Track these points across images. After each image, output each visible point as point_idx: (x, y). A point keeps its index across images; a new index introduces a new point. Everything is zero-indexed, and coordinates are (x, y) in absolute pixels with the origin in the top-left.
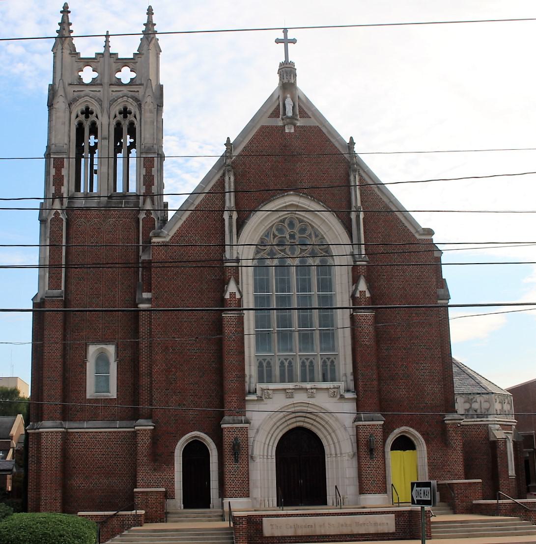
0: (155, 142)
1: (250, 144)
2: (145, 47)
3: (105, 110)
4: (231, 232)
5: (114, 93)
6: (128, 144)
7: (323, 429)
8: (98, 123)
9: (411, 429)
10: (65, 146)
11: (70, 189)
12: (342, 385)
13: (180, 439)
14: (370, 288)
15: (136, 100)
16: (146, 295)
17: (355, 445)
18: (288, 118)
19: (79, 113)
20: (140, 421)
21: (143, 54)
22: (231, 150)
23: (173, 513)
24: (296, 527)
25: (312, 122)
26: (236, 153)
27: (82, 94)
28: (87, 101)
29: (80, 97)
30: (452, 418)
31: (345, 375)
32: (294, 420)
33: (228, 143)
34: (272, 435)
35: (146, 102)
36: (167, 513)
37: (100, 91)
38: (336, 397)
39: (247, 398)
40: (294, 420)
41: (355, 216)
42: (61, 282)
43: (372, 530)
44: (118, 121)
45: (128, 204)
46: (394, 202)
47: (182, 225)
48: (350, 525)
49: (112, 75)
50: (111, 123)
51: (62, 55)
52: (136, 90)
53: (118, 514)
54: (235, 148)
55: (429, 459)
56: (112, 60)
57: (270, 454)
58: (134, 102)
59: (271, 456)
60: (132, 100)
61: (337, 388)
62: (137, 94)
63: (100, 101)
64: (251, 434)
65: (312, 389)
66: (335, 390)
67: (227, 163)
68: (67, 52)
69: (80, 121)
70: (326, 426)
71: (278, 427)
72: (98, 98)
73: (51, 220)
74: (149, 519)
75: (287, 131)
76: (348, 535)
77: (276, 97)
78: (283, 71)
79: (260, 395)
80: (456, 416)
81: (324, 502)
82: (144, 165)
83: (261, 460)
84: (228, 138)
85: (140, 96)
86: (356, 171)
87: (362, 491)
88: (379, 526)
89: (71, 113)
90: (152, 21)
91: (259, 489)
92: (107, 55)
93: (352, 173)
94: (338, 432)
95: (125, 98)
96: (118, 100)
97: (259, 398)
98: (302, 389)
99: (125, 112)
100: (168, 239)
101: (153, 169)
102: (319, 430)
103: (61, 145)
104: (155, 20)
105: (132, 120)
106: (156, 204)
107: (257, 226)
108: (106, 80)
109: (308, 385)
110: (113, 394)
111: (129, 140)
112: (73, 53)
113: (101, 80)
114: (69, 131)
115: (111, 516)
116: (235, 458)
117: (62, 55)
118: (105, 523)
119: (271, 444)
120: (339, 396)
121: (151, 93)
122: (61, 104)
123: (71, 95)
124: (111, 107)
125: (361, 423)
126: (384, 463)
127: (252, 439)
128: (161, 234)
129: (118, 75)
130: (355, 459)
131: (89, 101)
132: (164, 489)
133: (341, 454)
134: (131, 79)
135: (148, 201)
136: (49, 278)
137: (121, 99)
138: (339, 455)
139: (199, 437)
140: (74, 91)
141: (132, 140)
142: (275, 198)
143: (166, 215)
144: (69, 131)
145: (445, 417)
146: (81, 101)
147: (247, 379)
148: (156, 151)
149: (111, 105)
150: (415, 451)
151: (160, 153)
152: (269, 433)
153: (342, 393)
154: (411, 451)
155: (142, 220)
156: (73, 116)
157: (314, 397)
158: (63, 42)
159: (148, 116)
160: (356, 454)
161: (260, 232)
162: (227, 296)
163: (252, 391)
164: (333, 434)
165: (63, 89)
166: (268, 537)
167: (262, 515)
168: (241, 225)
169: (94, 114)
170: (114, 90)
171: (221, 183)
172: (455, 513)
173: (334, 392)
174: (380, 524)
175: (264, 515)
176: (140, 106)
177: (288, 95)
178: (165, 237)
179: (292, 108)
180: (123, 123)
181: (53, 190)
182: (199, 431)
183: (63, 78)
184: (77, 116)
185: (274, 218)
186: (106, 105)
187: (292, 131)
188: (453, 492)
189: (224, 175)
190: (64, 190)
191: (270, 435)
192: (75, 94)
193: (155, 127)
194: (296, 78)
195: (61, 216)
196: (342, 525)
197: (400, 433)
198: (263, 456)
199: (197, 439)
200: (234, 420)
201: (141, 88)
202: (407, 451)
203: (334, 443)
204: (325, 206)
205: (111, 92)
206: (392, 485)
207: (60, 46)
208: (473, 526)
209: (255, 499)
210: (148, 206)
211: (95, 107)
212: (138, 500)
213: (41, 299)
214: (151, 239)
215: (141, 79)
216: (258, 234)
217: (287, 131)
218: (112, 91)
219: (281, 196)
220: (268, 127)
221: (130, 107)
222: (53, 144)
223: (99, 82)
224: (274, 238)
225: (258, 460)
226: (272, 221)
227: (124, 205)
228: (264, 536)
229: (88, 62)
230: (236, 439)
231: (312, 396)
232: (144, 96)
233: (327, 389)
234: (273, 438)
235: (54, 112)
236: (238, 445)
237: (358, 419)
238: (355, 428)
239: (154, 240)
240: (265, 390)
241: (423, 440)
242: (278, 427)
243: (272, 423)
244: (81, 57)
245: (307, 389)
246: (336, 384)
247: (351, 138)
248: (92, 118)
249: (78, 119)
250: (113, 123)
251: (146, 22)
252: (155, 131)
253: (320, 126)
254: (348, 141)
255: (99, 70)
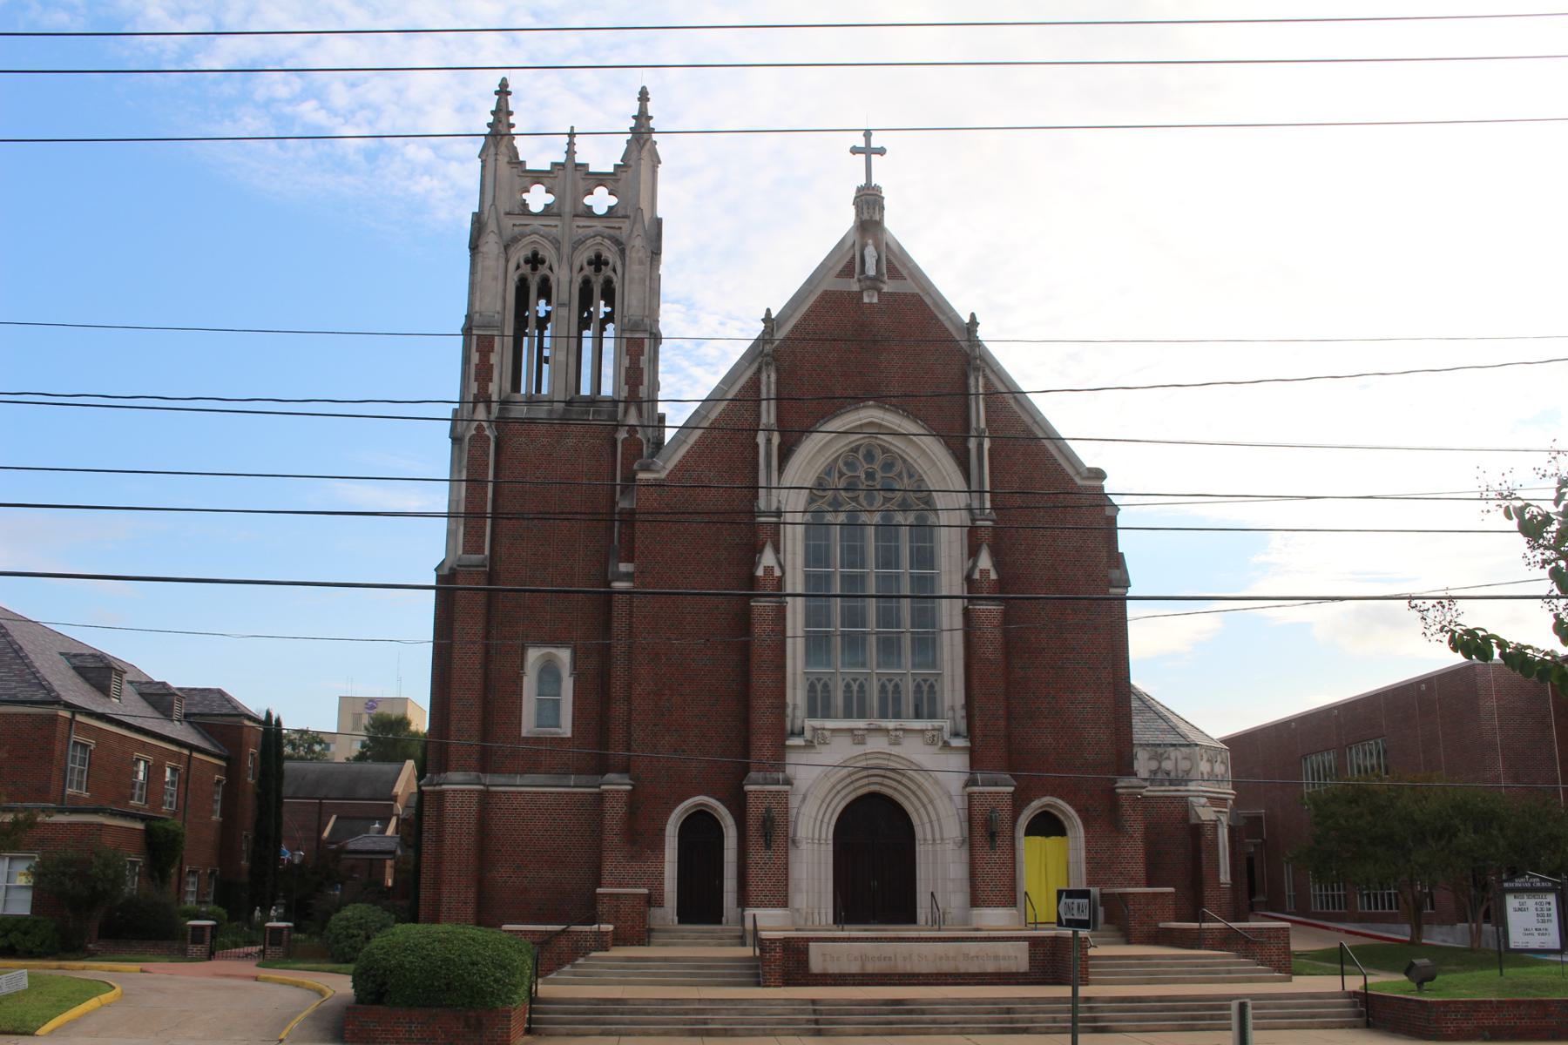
0: (647, 313)
1: (805, 320)
2: (634, 155)
3: (565, 258)
4: (768, 465)
5: (580, 231)
6: (602, 316)
7: (913, 798)
8: (553, 279)
9: (1060, 802)
10: (496, 316)
11: (503, 388)
12: (947, 725)
13: (676, 806)
14: (997, 565)
15: (617, 242)
16: (624, 567)
17: (966, 825)
18: (868, 278)
19: (522, 262)
20: (610, 776)
21: (630, 166)
22: (773, 330)
23: (660, 931)
24: (864, 958)
25: (908, 287)
26: (781, 334)
27: (527, 230)
28: (535, 241)
29: (523, 235)
30: (1129, 785)
31: (953, 708)
32: (866, 781)
33: (767, 319)
34: (828, 806)
35: (634, 246)
36: (651, 930)
37: (556, 226)
38: (935, 745)
39: (789, 743)
40: (866, 781)
41: (976, 445)
42: (484, 542)
43: (990, 967)
44: (586, 276)
45: (599, 415)
46: (1041, 423)
47: (688, 452)
48: (955, 958)
49: (577, 200)
50: (574, 280)
51: (496, 165)
52: (617, 225)
53: (568, 929)
54: (779, 327)
55: (1088, 852)
56: (579, 175)
57: (824, 836)
58: (613, 245)
59: (826, 840)
60: (609, 242)
61: (939, 730)
62: (618, 232)
63: (556, 243)
64: (794, 802)
65: (896, 730)
66: (936, 733)
67: (765, 352)
68: (503, 160)
69: (522, 274)
70: (920, 793)
71: (838, 792)
72: (554, 238)
73: (470, 439)
74: (620, 939)
75: (866, 300)
76: (951, 974)
77: (849, 243)
78: (861, 200)
79: (809, 738)
80: (1134, 781)
81: (911, 918)
82: (628, 350)
83: (809, 845)
84: (768, 310)
85: (623, 235)
86: (979, 371)
87: (975, 902)
88: (1002, 962)
89: (507, 261)
90: (646, 112)
91: (805, 894)
92: (570, 167)
93: (972, 372)
94: (938, 802)
95: (599, 239)
96: (588, 241)
97: (809, 744)
98: (879, 730)
99: (598, 262)
100: (663, 475)
101: (642, 358)
102: (907, 798)
103: (491, 314)
104: (652, 109)
105: (609, 277)
106: (646, 417)
107: (813, 457)
108: (568, 208)
109: (891, 724)
110: (566, 729)
111: (603, 309)
112: (514, 161)
113: (559, 208)
114: (505, 290)
115: (557, 933)
116: (766, 841)
117: (496, 165)
118: (546, 944)
119: (826, 820)
120: (940, 744)
121: (641, 232)
122: (491, 245)
123: (509, 232)
124: (575, 254)
125: (975, 789)
126: (1014, 858)
127: (796, 810)
128: (653, 467)
129: (588, 200)
130: (966, 846)
131: (539, 243)
132: (646, 891)
133: (942, 839)
134: (546, 205)
135: (633, 411)
136: (464, 534)
137: (592, 240)
138: (939, 842)
139: (712, 808)
140: (514, 225)
141: (608, 309)
142: (842, 411)
143: (661, 435)
144: (505, 290)
145: (1116, 783)
146: (525, 241)
147: (789, 711)
148: (648, 328)
149: (574, 249)
150: (1065, 837)
151: (654, 331)
152: (823, 802)
153: (946, 738)
154: (1059, 837)
155: (622, 442)
156: (512, 266)
157: (899, 744)
158: (498, 143)
159: (635, 270)
160: (967, 839)
161: (817, 466)
162: (760, 572)
163: (796, 730)
164: (930, 807)
165: (495, 221)
166: (816, 975)
167: (807, 938)
168: (785, 454)
169: (547, 264)
170: (581, 224)
171: (755, 383)
172: (1129, 942)
173: (934, 736)
174: (1004, 958)
175: (812, 938)
176: (622, 252)
177: (870, 241)
178: (658, 472)
179: (875, 262)
180: (593, 279)
181: (474, 388)
182: (707, 795)
183: (497, 203)
184: (518, 267)
185: (842, 444)
186: (566, 249)
187: (875, 300)
188: (1126, 906)
189: (759, 370)
190: (493, 388)
191: (825, 805)
192: (516, 229)
193: (648, 289)
194: (883, 212)
195: (487, 432)
196: (941, 958)
197: (1041, 807)
198: (813, 839)
199: (703, 808)
200: (766, 779)
201: (624, 222)
202: (1053, 838)
203: (931, 822)
204: (925, 426)
205: (575, 229)
206: (1026, 893)
207: (492, 150)
208: (1158, 965)
209: (798, 910)
210: (632, 420)
211: (548, 252)
212: (602, 908)
213: (451, 569)
214: (635, 473)
215: (626, 209)
216: (814, 470)
217: (866, 300)
218: (578, 227)
219: (853, 407)
220: (834, 293)
221: (606, 254)
222: (476, 312)
223: (555, 210)
224: (839, 478)
225: (804, 846)
226: (837, 451)
227: (593, 416)
228: (811, 972)
229: (538, 177)
230: (768, 810)
231: (896, 742)
232: (630, 236)
233: (922, 731)
234: (830, 810)
235: (479, 259)
236: (772, 820)
237: (971, 782)
238: (966, 798)
239: (642, 476)
240: (818, 729)
241: (1079, 820)
242: (838, 792)
243: (828, 785)
244: (528, 168)
245: (887, 730)
246: (936, 723)
247: (973, 315)
248: (543, 270)
249: (520, 272)
250: (578, 279)
251: (636, 114)
252: (647, 295)
253: (921, 294)
254: (967, 319)
255: (556, 189)
